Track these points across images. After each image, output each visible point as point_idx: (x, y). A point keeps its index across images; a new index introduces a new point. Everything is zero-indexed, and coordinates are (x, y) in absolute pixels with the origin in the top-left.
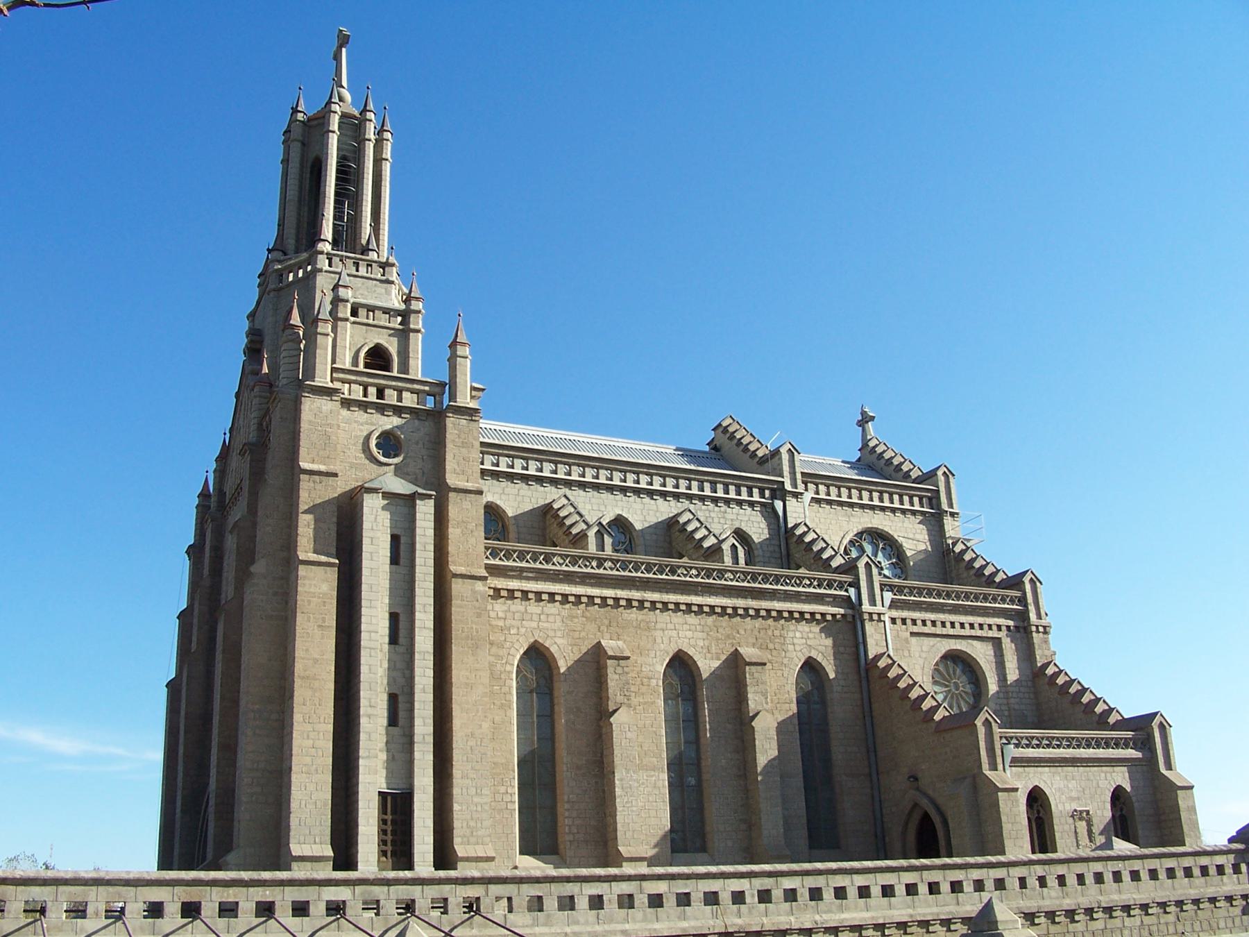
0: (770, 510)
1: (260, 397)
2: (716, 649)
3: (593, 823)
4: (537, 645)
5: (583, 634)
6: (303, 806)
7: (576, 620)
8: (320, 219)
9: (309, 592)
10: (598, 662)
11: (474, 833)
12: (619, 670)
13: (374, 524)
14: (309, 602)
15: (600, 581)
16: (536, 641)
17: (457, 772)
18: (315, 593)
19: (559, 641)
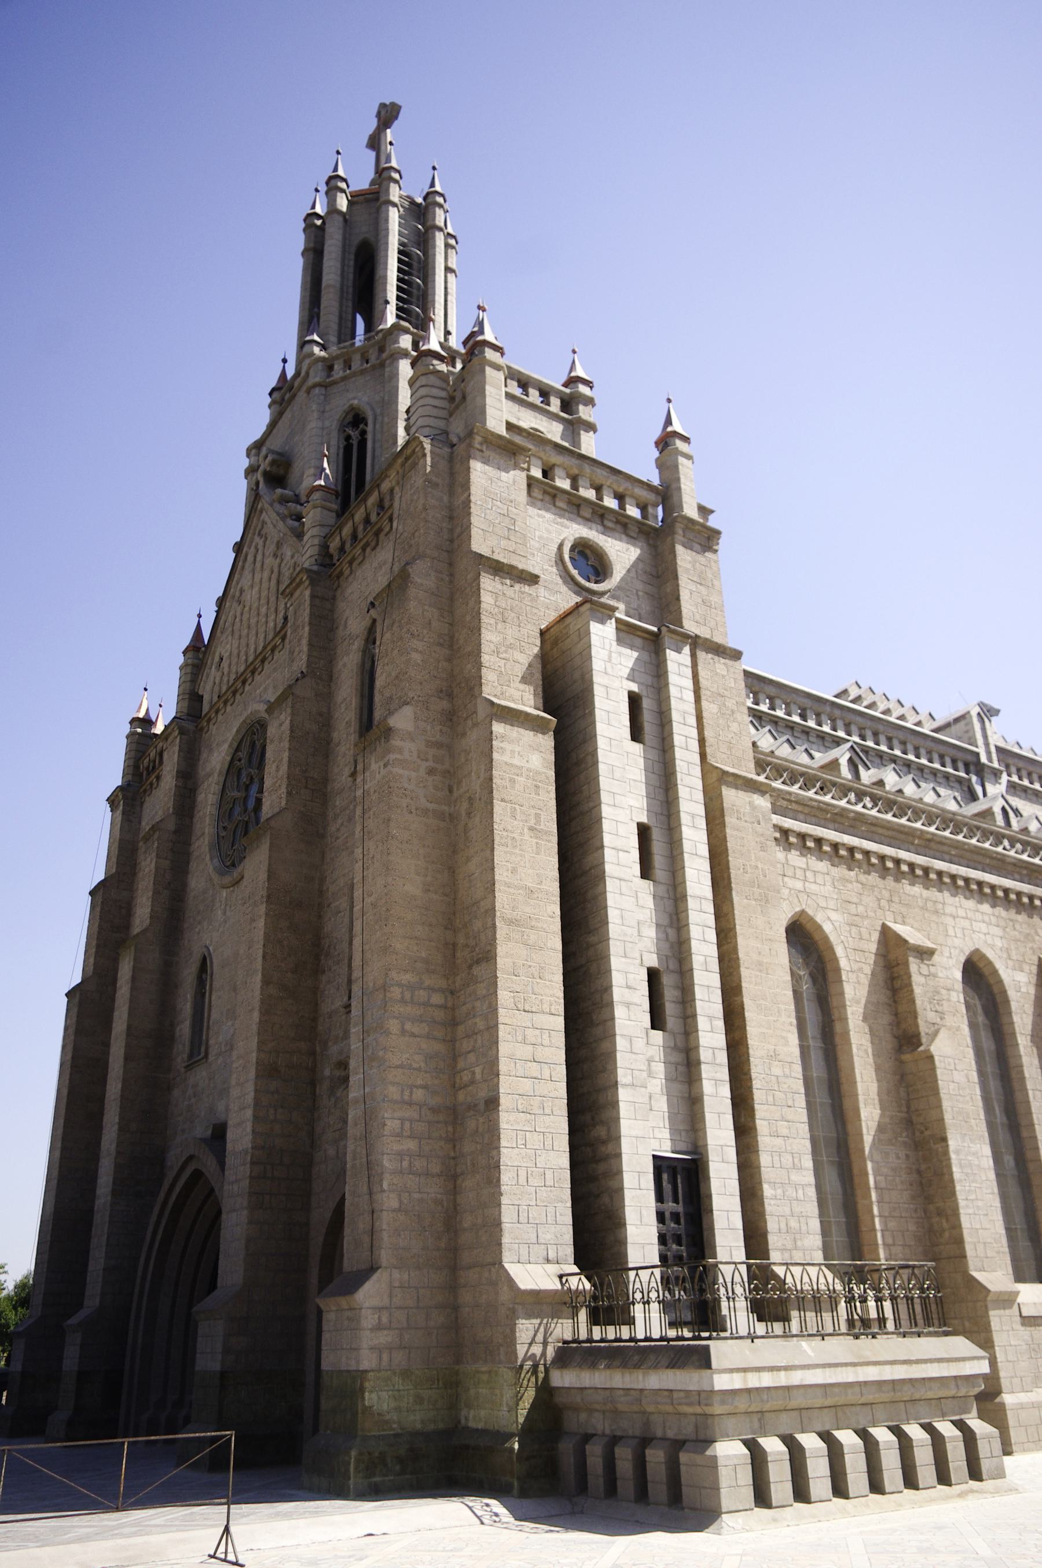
0: (966, 789)
1: (323, 507)
2: (1017, 954)
3: (912, 1227)
4: (803, 921)
5: (861, 909)
6: (522, 1180)
7: (850, 886)
8: (381, 307)
9: (512, 765)
10: (451, 1041)
11: (799, 1243)
12: (924, 970)
13: (608, 665)
14: (512, 781)
15: (874, 829)
16: (803, 912)
17: (762, 1126)
18: (520, 768)
19: (834, 916)
